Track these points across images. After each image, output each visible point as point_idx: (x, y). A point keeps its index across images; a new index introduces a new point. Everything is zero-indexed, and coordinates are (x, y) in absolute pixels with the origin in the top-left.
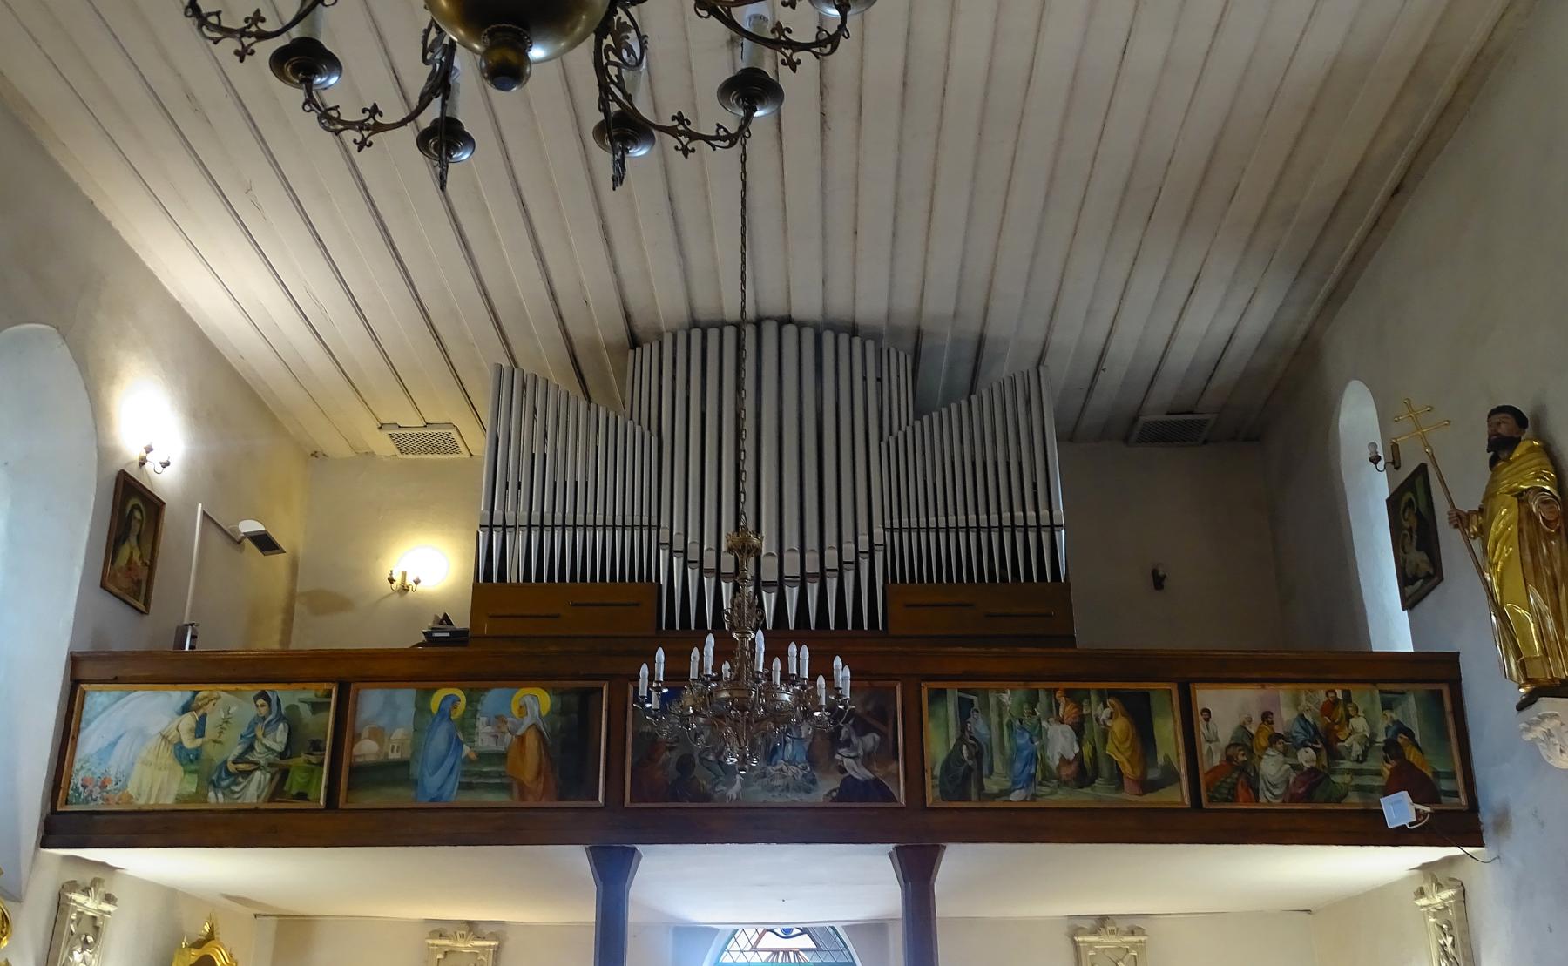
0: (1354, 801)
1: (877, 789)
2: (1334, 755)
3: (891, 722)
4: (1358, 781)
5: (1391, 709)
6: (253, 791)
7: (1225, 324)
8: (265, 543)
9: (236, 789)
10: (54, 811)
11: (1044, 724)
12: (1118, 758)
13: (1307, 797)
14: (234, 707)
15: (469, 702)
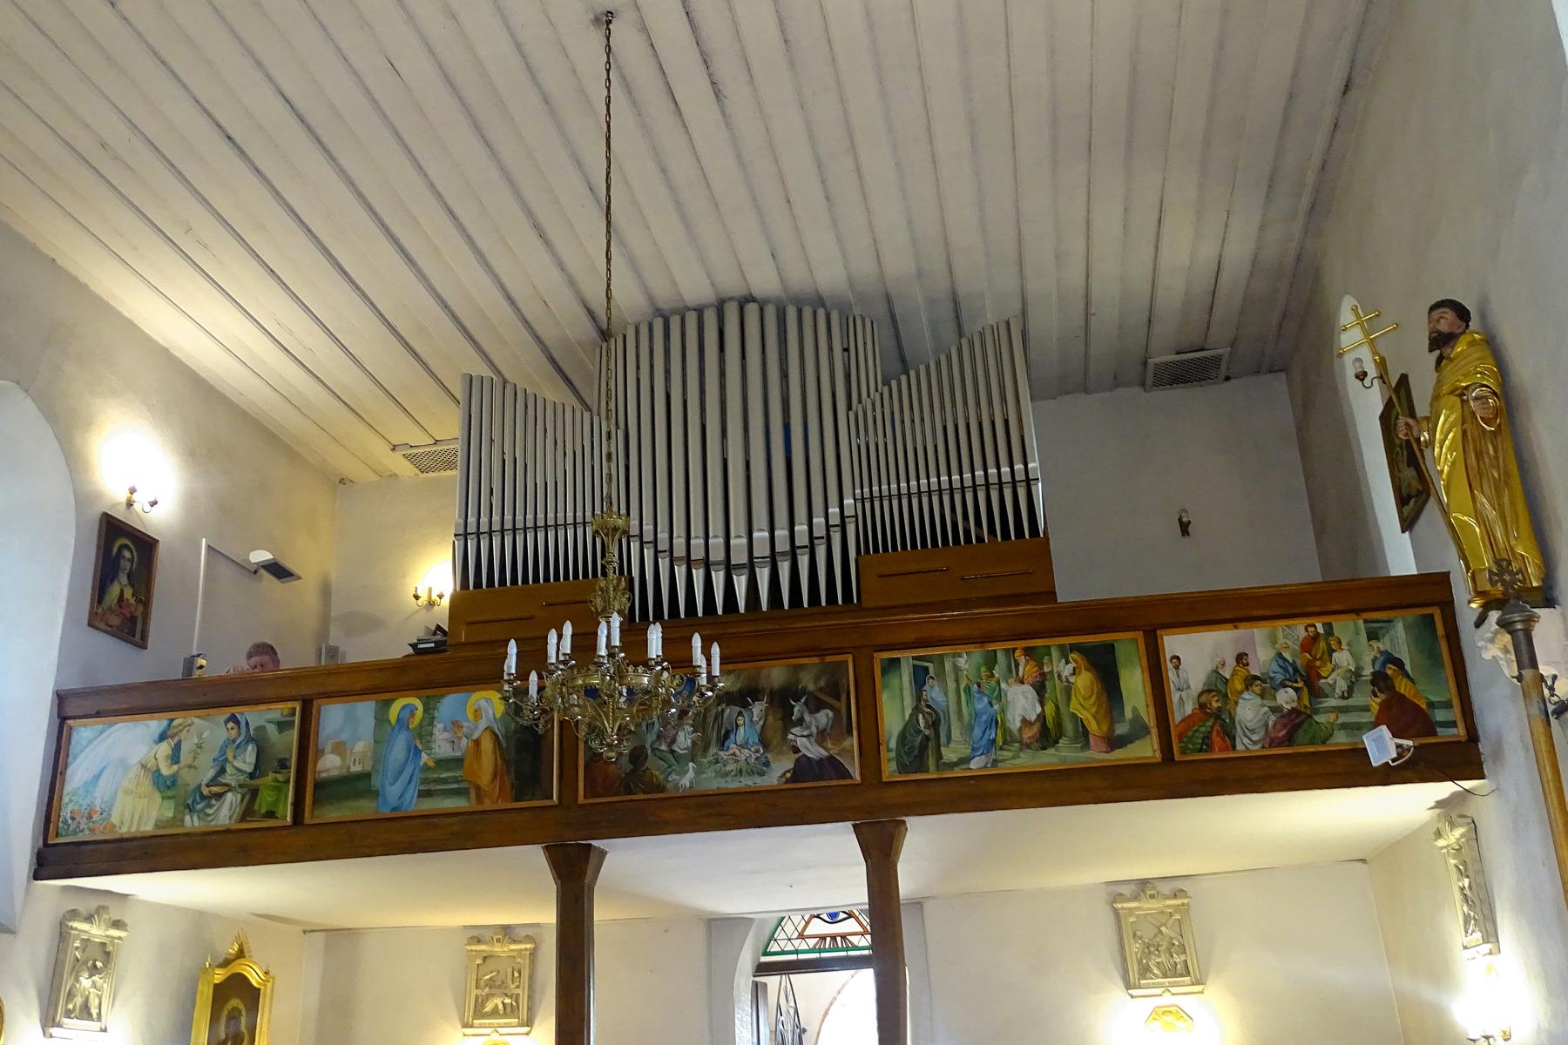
0: (1341, 739)
1: (832, 766)
2: (1316, 693)
3: (844, 697)
4: (1343, 719)
5: (1377, 639)
6: (225, 813)
7: (1208, 250)
8: (278, 571)
9: (210, 811)
10: (45, 844)
11: (1003, 685)
12: (1084, 715)
13: (1289, 740)
14: (206, 732)
15: (426, 710)
